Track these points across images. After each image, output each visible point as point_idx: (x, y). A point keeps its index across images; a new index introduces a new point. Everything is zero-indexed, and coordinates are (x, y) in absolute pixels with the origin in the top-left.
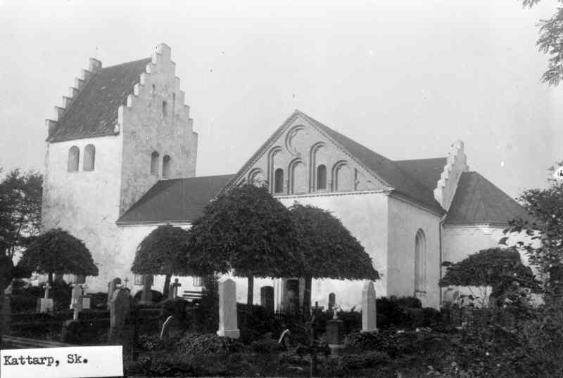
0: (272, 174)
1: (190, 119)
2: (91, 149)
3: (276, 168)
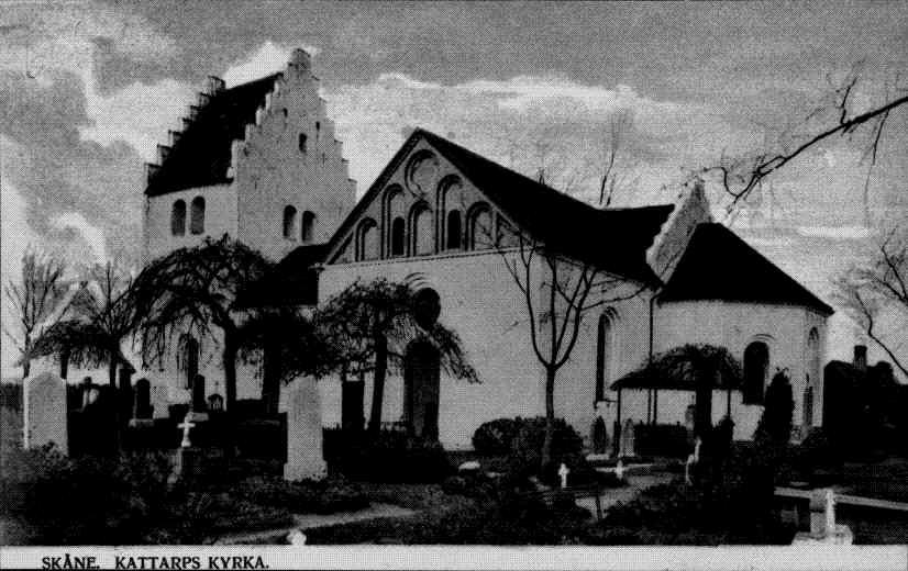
0: (389, 225)
1: (343, 160)
2: (199, 203)
3: (394, 216)
